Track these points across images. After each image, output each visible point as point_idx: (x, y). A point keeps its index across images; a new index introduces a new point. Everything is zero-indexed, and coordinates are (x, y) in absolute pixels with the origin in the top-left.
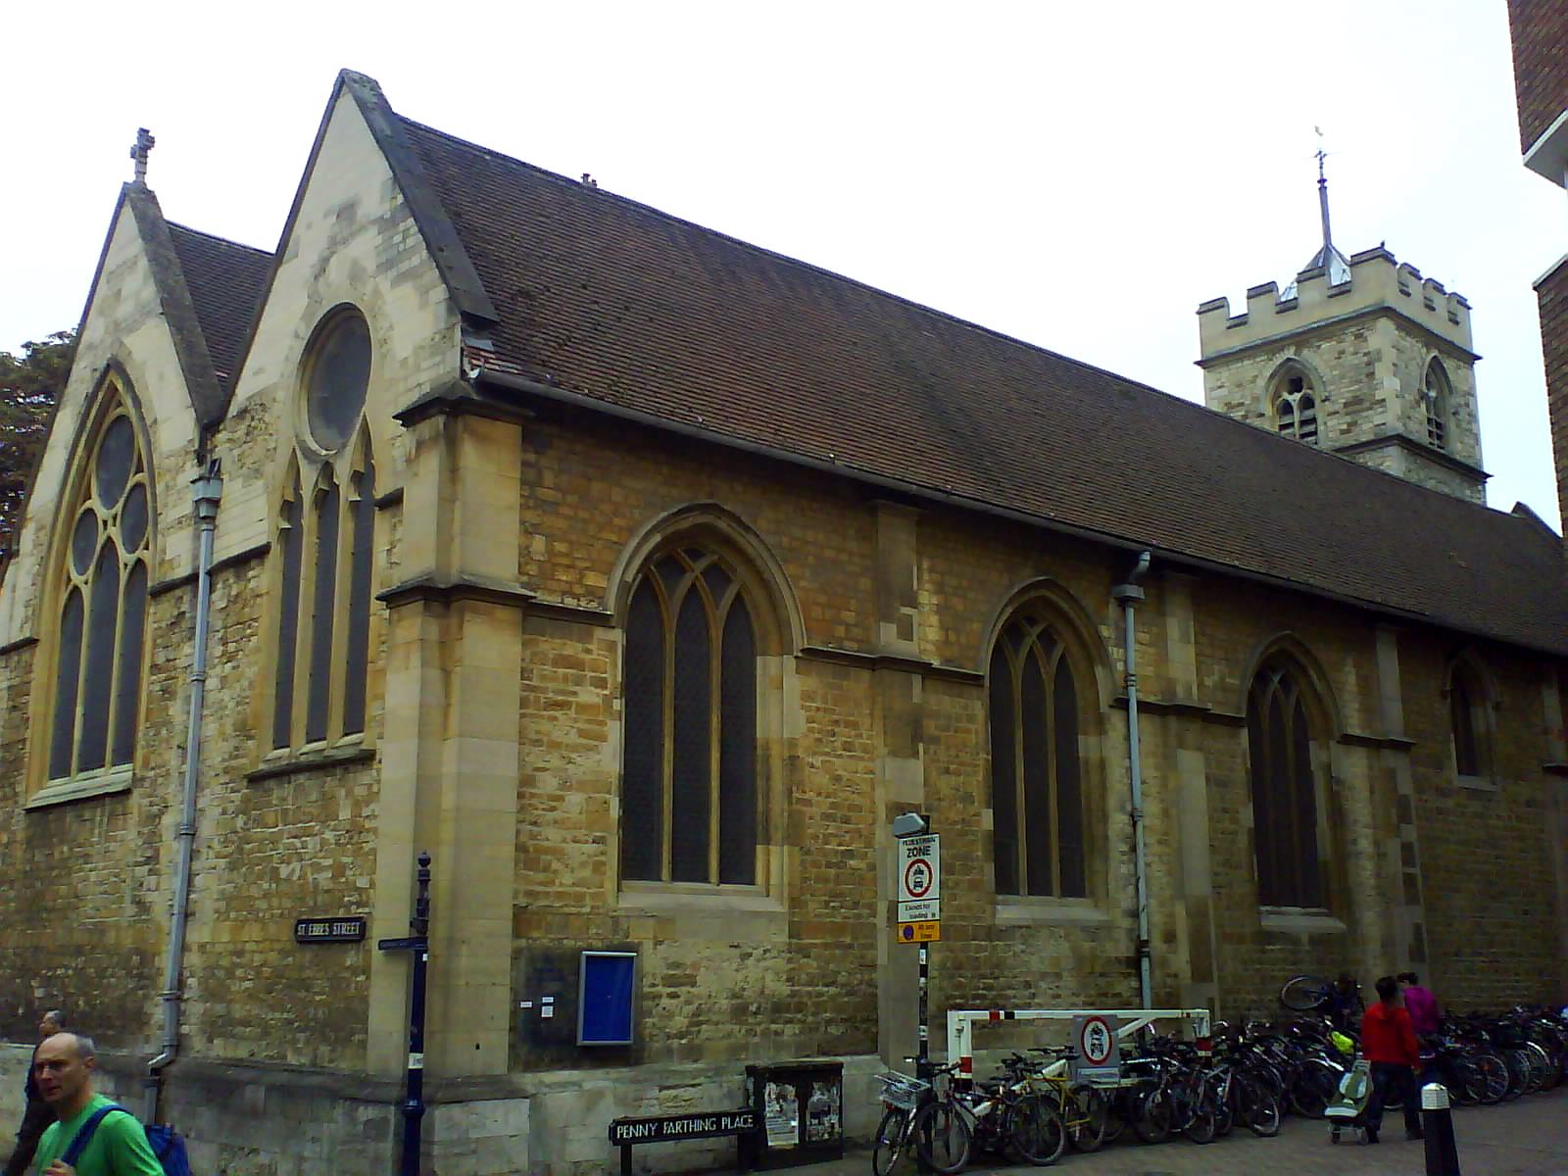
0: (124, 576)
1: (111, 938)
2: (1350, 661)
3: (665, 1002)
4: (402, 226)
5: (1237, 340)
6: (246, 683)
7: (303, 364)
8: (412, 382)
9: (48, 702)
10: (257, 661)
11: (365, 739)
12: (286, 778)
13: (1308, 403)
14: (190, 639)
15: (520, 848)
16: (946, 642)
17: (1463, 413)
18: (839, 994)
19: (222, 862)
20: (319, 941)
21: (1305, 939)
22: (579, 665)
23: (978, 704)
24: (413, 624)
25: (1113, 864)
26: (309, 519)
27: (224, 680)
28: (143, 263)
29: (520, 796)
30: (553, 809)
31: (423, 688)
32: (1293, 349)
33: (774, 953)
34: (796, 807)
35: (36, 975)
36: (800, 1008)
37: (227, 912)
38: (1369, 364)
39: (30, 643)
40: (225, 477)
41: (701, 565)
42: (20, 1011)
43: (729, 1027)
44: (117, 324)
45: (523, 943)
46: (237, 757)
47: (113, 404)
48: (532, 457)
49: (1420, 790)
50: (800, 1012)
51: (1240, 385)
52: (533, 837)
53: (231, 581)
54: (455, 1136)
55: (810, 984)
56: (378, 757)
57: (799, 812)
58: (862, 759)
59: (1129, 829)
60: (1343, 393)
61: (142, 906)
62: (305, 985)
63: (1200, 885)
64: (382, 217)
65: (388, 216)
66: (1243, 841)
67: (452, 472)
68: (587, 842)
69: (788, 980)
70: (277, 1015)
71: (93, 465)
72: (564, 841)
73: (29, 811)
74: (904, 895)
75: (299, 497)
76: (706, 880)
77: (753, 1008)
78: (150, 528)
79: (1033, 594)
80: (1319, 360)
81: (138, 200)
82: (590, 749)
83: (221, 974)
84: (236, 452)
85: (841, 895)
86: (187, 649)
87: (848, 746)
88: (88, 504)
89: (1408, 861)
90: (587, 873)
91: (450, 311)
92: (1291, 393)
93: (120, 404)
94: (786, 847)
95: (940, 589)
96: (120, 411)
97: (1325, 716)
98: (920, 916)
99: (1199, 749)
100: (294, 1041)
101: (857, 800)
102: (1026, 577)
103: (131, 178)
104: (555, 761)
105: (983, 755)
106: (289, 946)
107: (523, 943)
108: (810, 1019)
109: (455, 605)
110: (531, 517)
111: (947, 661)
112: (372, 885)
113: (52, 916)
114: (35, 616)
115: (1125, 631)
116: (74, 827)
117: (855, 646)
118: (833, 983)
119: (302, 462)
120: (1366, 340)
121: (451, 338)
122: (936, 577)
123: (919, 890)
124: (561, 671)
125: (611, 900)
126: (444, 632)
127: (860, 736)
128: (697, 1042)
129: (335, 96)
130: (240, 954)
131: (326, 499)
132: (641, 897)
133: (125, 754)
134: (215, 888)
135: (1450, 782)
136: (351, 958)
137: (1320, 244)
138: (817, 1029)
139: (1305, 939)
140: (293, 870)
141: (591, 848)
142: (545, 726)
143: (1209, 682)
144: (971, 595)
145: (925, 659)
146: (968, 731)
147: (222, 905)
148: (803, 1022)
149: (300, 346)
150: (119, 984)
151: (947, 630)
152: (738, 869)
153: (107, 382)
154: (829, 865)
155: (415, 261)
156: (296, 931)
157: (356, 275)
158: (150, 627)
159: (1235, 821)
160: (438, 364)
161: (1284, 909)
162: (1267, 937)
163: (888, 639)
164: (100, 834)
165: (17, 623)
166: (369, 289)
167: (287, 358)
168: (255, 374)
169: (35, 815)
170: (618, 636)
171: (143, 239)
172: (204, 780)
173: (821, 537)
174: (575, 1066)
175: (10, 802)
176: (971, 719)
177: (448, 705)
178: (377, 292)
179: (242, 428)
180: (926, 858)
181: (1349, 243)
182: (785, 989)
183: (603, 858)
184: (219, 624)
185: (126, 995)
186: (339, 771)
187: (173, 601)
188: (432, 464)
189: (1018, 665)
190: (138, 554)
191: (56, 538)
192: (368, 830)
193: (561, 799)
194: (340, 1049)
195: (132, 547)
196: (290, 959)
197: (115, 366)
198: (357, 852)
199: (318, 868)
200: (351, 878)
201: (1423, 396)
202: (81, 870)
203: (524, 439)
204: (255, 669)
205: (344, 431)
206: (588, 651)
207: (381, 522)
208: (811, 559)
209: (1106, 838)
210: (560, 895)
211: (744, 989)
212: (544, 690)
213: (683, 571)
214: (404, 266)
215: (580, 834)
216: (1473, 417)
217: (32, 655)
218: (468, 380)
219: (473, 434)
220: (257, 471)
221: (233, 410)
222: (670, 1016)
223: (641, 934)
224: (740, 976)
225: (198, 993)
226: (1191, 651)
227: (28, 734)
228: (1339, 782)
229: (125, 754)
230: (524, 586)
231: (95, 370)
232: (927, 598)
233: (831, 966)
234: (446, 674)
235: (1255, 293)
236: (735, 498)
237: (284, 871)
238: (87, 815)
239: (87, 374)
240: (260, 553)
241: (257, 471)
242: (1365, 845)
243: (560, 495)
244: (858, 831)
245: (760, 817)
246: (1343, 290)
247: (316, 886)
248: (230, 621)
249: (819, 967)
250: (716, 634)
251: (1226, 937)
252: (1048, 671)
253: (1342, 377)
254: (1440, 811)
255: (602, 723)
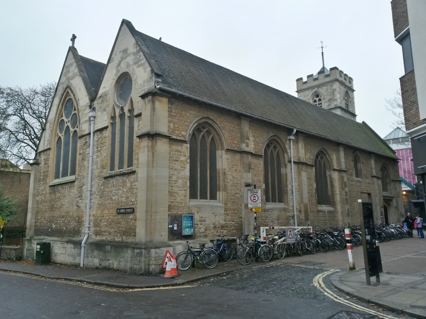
0: (71, 134)
1: (71, 214)
2: (334, 153)
3: (199, 225)
4: (139, 54)
5: (305, 86)
6: (103, 157)
7: (115, 86)
8: (143, 89)
9: (53, 162)
10: (106, 152)
11: (133, 168)
12: (113, 178)
13: (320, 100)
14: (89, 147)
15: (169, 192)
16: (255, 148)
17: (352, 102)
18: (235, 224)
19: (98, 197)
20: (123, 213)
21: (326, 212)
22: (181, 152)
23: (262, 161)
24: (145, 142)
25: (289, 196)
26: (118, 120)
27: (97, 156)
28: (75, 64)
29: (169, 180)
30: (176, 183)
31: (148, 157)
32: (317, 88)
33: (222, 215)
34: (225, 183)
35: (53, 222)
36: (227, 227)
37: (100, 207)
38: (333, 91)
39: (49, 149)
40: (97, 111)
41: (205, 130)
42: (50, 230)
43: (212, 231)
44: (68, 78)
45: (170, 213)
46: (101, 173)
47: (68, 95)
48: (170, 106)
49: (348, 181)
50: (227, 227)
51: (305, 96)
52: (171, 189)
53: (99, 134)
54: (157, 256)
55: (229, 221)
56: (136, 172)
57: (226, 184)
58: (238, 173)
59: (292, 188)
60: (328, 98)
61: (78, 207)
62: (119, 223)
63: (306, 201)
64: (134, 52)
65: (135, 52)
66: (314, 191)
67: (153, 109)
68: (183, 191)
69: (224, 221)
70: (112, 230)
71: (63, 109)
72: (178, 190)
73: (50, 186)
74: (250, 201)
75: (115, 116)
76: (207, 199)
77: (217, 227)
78: (78, 122)
79: (272, 138)
80: (322, 91)
81: (72, 50)
82: (183, 170)
83: (99, 221)
84: (99, 106)
85: (235, 202)
86: (88, 150)
87: (236, 170)
88: (62, 118)
89: (346, 196)
90: (183, 197)
91: (152, 73)
92: (316, 98)
93: (69, 96)
94: (224, 192)
95: (254, 136)
96: (69, 97)
97: (330, 165)
98: (255, 206)
99: (306, 171)
100: (117, 235)
101: (239, 182)
102: (271, 134)
103: (71, 45)
104: (176, 173)
105: (263, 172)
106: (115, 214)
107: (170, 213)
108: (229, 229)
109: (154, 138)
110: (170, 119)
111: (256, 152)
112: (136, 200)
113: (56, 209)
114: (50, 143)
115: (290, 146)
116: (61, 190)
117: (237, 148)
118: (233, 221)
119: (116, 108)
120: (333, 86)
121: (152, 79)
122: (253, 134)
123: (255, 201)
124: (177, 153)
125: (188, 203)
126: (153, 144)
127: (238, 168)
128: (206, 234)
129: (122, 25)
130: (103, 217)
131: (122, 116)
132: (194, 202)
133: (73, 173)
134: (97, 203)
135: (354, 179)
136: (131, 216)
137: (322, 66)
138: (230, 231)
139: (326, 212)
140: (116, 198)
141: (184, 192)
142: (174, 165)
143: (307, 157)
144: (260, 138)
145: (252, 151)
146: (260, 167)
147: (98, 206)
148: (228, 230)
149: (114, 82)
150: (73, 224)
151: (255, 145)
152: (213, 197)
153: (66, 91)
154: (232, 196)
155: (143, 62)
156: (117, 211)
157: (128, 66)
158: (79, 145)
159: (312, 187)
160: (149, 85)
161: (322, 205)
162: (319, 211)
163: (244, 147)
164: (67, 191)
165: (46, 145)
166: (131, 68)
167: (111, 84)
168: (103, 88)
169: (52, 187)
170: (188, 145)
171: (74, 58)
172: (93, 179)
173: (230, 125)
174: (181, 240)
175: (45, 185)
176: (260, 165)
177: (153, 160)
178: (133, 69)
179: (101, 100)
180: (257, 194)
181: (328, 67)
182: (224, 223)
183: (186, 194)
184: (96, 144)
185: (75, 226)
186: (127, 176)
187: (84, 139)
188: (149, 106)
189: (269, 153)
190: (76, 129)
191: (55, 126)
192: (134, 188)
193: (177, 181)
194: (128, 237)
195: (73, 127)
196: (116, 217)
197: (68, 87)
198: (132, 193)
199: (122, 197)
200: (130, 199)
201: (344, 98)
202: (63, 199)
203: (169, 102)
204: (105, 153)
205: (126, 101)
206: (182, 149)
207: (136, 121)
208: (228, 130)
209: (287, 190)
210: (177, 202)
211: (215, 223)
212: (173, 157)
213: (201, 132)
214: (140, 63)
215: (181, 189)
216: (354, 103)
217: (50, 152)
218: (156, 88)
219: (158, 100)
220: (105, 110)
221: (98, 96)
222: (201, 228)
223: (194, 211)
224: (214, 220)
225: (93, 226)
226: (304, 150)
227: (49, 169)
228: (333, 179)
229: (73, 173)
230: (169, 134)
231: (63, 88)
232: (251, 139)
233: (233, 218)
234: (153, 153)
235: (308, 77)
236: (213, 116)
237: (114, 198)
238: (64, 187)
239: (61, 89)
240: (106, 128)
241: (105, 110)
242: (338, 192)
243: (176, 114)
244: (238, 189)
245: (218, 186)
246: (328, 76)
247: (122, 201)
248: (99, 143)
249: (231, 218)
250: (208, 145)
251: (311, 212)
252: (275, 154)
253: (327, 94)
254: (352, 185)
255: (185, 165)
